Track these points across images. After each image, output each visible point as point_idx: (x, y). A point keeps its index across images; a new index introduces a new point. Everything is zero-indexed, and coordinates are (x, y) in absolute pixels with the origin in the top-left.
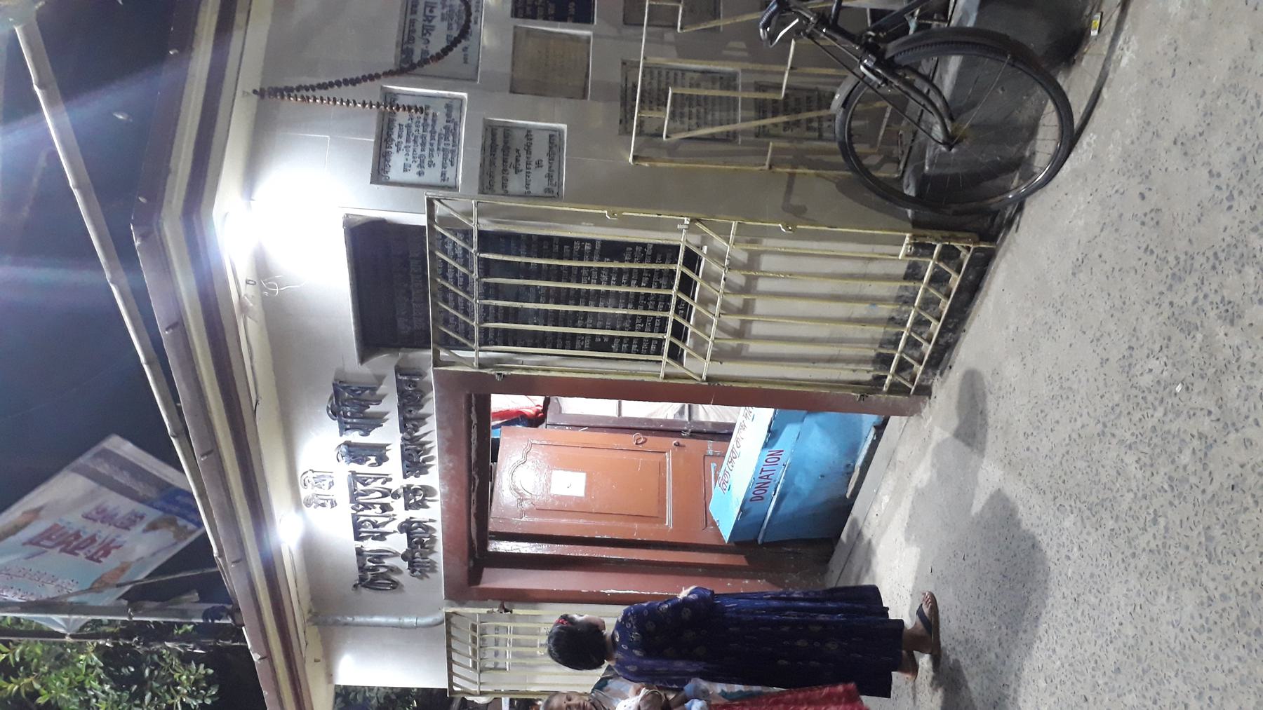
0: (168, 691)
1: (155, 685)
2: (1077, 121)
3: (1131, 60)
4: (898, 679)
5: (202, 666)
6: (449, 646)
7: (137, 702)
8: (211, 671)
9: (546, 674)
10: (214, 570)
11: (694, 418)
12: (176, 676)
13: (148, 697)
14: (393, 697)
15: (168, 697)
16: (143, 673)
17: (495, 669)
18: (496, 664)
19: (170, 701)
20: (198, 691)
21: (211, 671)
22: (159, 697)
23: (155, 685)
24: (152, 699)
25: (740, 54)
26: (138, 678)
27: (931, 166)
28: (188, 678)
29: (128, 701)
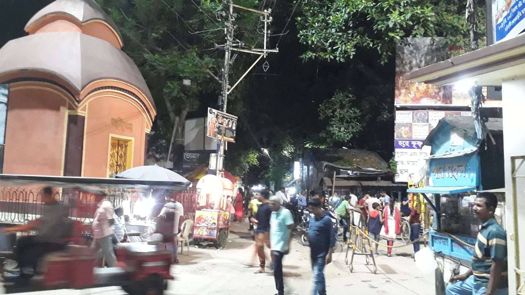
0: (343, 41)
1: (345, 36)
5: (354, 53)
7: (338, 30)
8: (351, 57)
10: (132, 166)
12: (349, 44)
13: (341, 34)
14: (447, 95)
16: (349, 30)
17: (501, 218)
19: (339, 43)
20: (342, 54)
21: (351, 57)
22: (339, 39)
23: (345, 36)
24: (339, 36)
26: (348, 28)
27: (274, 48)
29: (338, 26)
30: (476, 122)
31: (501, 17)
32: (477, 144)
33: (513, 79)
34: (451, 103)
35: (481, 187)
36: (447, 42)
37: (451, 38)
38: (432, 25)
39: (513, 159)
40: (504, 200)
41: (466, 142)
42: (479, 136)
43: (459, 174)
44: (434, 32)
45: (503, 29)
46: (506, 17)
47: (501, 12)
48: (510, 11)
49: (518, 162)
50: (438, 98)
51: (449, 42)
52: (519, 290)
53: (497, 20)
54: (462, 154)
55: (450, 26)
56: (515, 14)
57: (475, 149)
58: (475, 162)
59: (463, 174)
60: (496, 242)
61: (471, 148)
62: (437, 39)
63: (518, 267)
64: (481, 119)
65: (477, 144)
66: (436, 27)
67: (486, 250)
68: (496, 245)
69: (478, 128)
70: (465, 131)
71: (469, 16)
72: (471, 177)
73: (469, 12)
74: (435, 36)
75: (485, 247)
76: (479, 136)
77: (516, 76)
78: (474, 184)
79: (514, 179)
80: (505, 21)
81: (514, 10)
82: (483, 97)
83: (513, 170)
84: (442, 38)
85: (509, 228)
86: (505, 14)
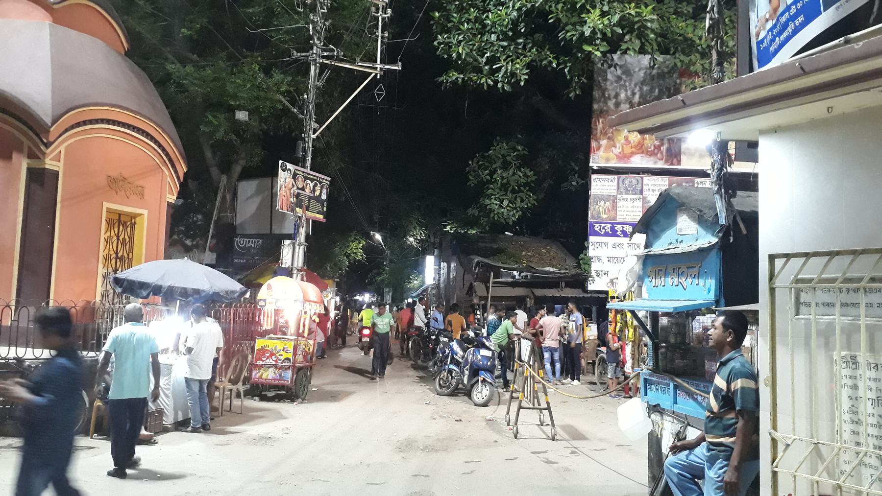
0: (508, 57)
1: (512, 48)
2: (809, 458)
3: (455, 83)
4: (15, 156)
5: (527, 77)
6: (838, 253)
8: (522, 84)
9: (811, 377)
11: (594, 177)
12: (519, 61)
13: (505, 44)
15: (504, 57)
16: (519, 38)
18: (809, 305)
21: (522, 84)
22: (503, 51)
24: (503, 47)
25: (815, 490)
26: (517, 34)
27: (394, 63)
28: (517, 69)
29: (502, 31)
30: (717, 196)
31: (764, 29)
32: (718, 232)
33: (775, 131)
34: (679, 163)
35: (722, 301)
36: (675, 65)
37: (682, 57)
38: (652, 36)
39: (772, 258)
40: (756, 322)
41: (700, 229)
42: (722, 221)
43: (689, 280)
44: (655, 47)
45: (767, 49)
46: (771, 30)
47: (764, 21)
48: (778, 20)
49: (779, 263)
50: (659, 155)
51: (679, 64)
52: (775, 464)
53: (758, 35)
54: (694, 248)
55: (681, 38)
56: (785, 26)
57: (714, 240)
58: (714, 261)
59: (696, 281)
60: (742, 383)
61: (708, 239)
62: (660, 58)
63: (775, 427)
64: (726, 192)
65: (718, 232)
66: (659, 39)
67: (727, 400)
68: (742, 388)
69: (720, 206)
70: (701, 211)
71: (710, 26)
72: (708, 286)
73: (711, 19)
74: (658, 53)
75: (723, 393)
76: (722, 221)
77: (779, 127)
78: (711, 297)
79: (772, 290)
80: (770, 37)
81: (783, 19)
82: (729, 156)
83: (772, 277)
84: (669, 57)
85: (764, 373)
86: (770, 25)
